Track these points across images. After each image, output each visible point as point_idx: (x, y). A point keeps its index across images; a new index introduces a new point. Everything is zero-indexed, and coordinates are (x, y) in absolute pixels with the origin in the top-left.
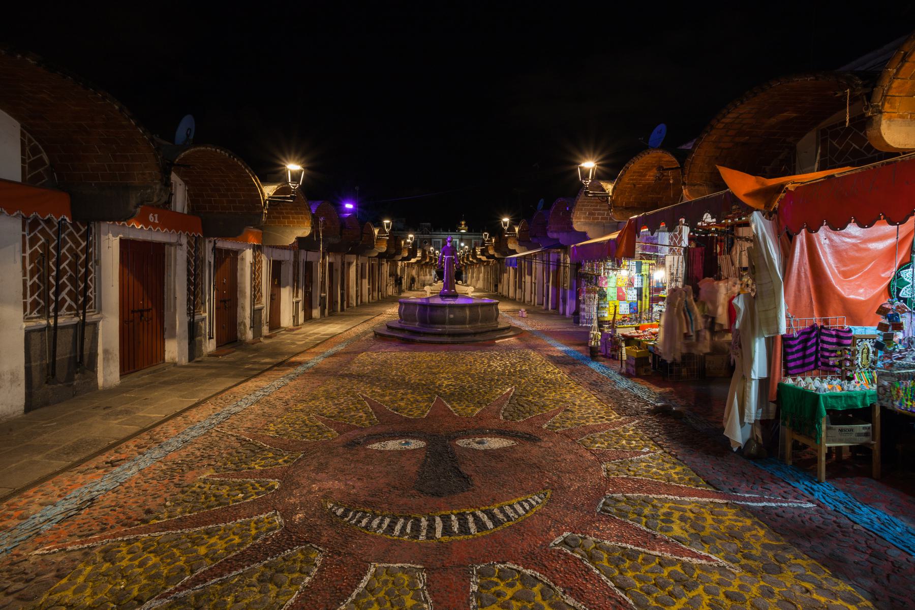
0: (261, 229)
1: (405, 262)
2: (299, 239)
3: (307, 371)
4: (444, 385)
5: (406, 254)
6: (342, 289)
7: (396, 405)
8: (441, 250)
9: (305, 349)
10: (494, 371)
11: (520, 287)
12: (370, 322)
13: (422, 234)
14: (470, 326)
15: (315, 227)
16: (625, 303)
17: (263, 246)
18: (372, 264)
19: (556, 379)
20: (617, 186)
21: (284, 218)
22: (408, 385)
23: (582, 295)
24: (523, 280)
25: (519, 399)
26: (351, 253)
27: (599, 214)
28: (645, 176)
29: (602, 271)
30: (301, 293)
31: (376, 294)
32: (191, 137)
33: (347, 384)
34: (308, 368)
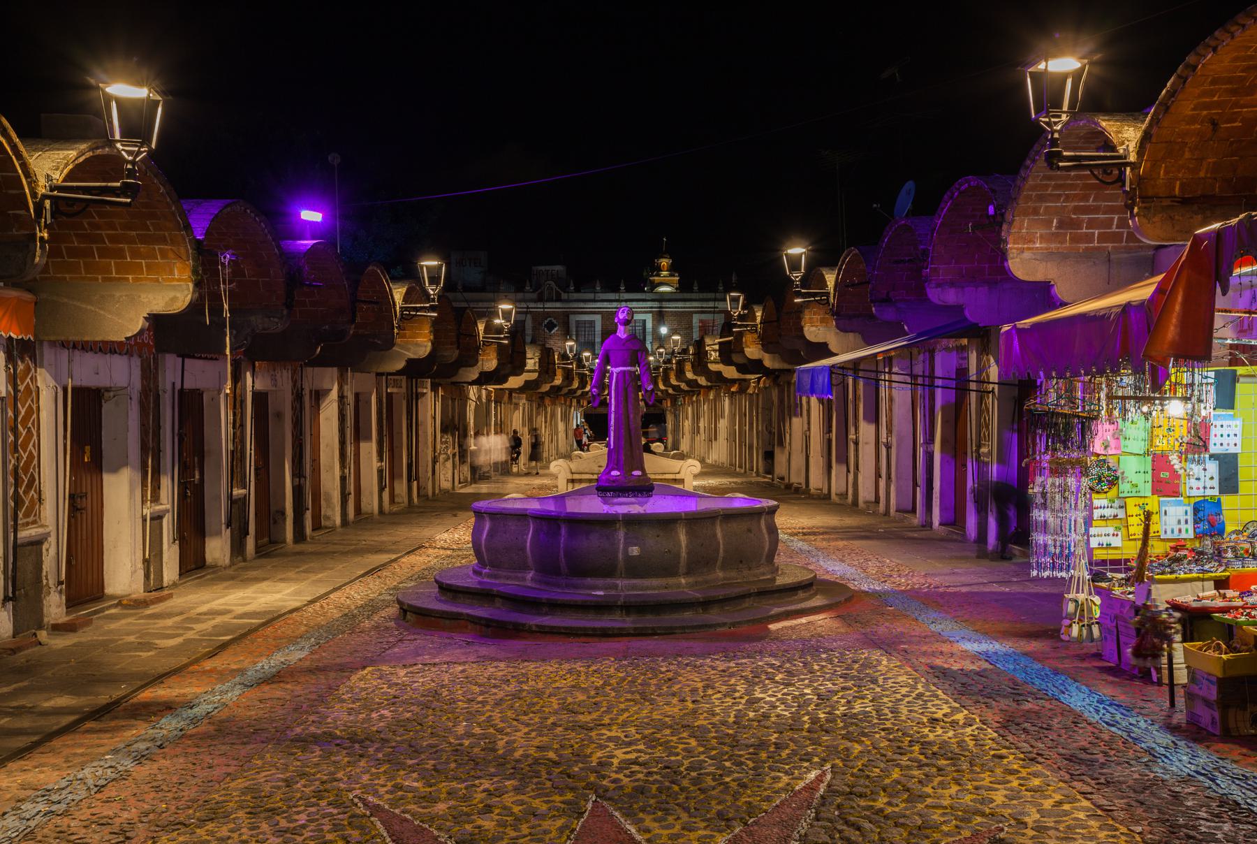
0: (29, 291)
1: (490, 388)
2: (157, 321)
3: (191, 730)
4: (615, 761)
5: (490, 362)
6: (298, 472)
7: (468, 827)
8: (598, 350)
9: (185, 660)
10: (766, 716)
11: (843, 459)
12: (385, 573)
13: (540, 299)
14: (691, 580)
15: (205, 279)
16: (1179, 504)
17: (41, 342)
18: (390, 396)
19: (961, 744)
20: (1154, 130)
21: (104, 253)
22: (504, 764)
23: (1039, 480)
24: (852, 436)
25: (847, 804)
26: (322, 362)
27: (1091, 224)
29: (1104, 403)
30: (168, 487)
31: (401, 487)
33: (317, 765)
34: (194, 721)
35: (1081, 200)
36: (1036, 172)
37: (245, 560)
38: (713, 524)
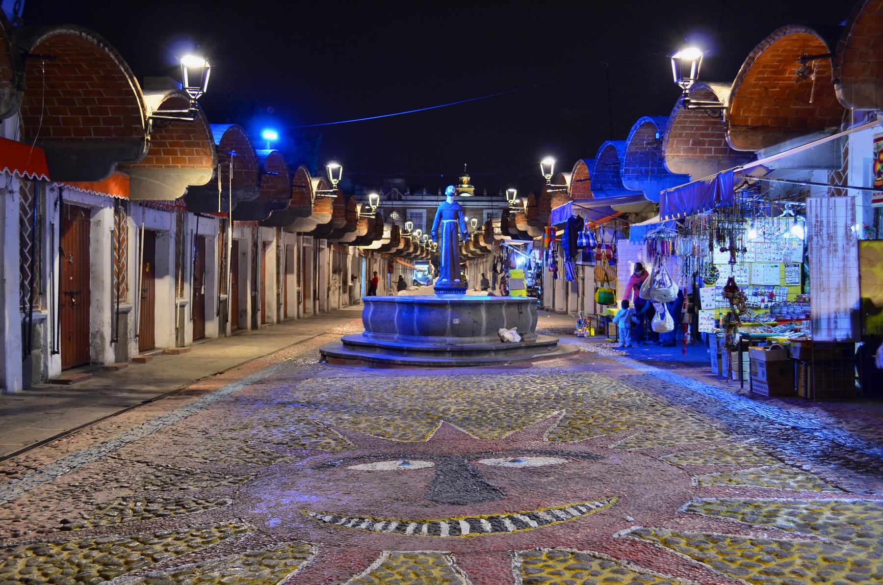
5: (363, 230)
11: (576, 290)
12: (307, 343)
14: (488, 338)
18: (304, 248)
21: (167, 152)
26: (269, 224)
27: (711, 143)
28: (783, 72)
31: (310, 304)
32: (20, 15)
35: (704, 130)
36: (679, 112)
37: (226, 336)
38: (501, 307)
